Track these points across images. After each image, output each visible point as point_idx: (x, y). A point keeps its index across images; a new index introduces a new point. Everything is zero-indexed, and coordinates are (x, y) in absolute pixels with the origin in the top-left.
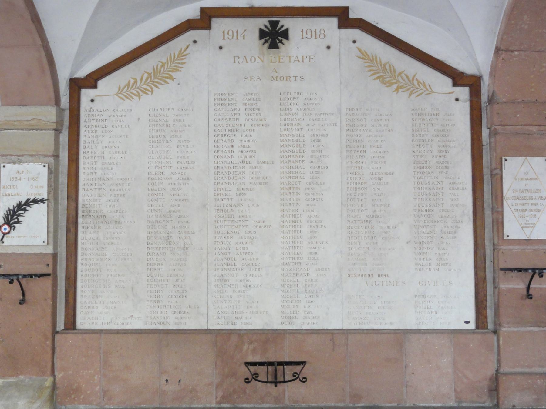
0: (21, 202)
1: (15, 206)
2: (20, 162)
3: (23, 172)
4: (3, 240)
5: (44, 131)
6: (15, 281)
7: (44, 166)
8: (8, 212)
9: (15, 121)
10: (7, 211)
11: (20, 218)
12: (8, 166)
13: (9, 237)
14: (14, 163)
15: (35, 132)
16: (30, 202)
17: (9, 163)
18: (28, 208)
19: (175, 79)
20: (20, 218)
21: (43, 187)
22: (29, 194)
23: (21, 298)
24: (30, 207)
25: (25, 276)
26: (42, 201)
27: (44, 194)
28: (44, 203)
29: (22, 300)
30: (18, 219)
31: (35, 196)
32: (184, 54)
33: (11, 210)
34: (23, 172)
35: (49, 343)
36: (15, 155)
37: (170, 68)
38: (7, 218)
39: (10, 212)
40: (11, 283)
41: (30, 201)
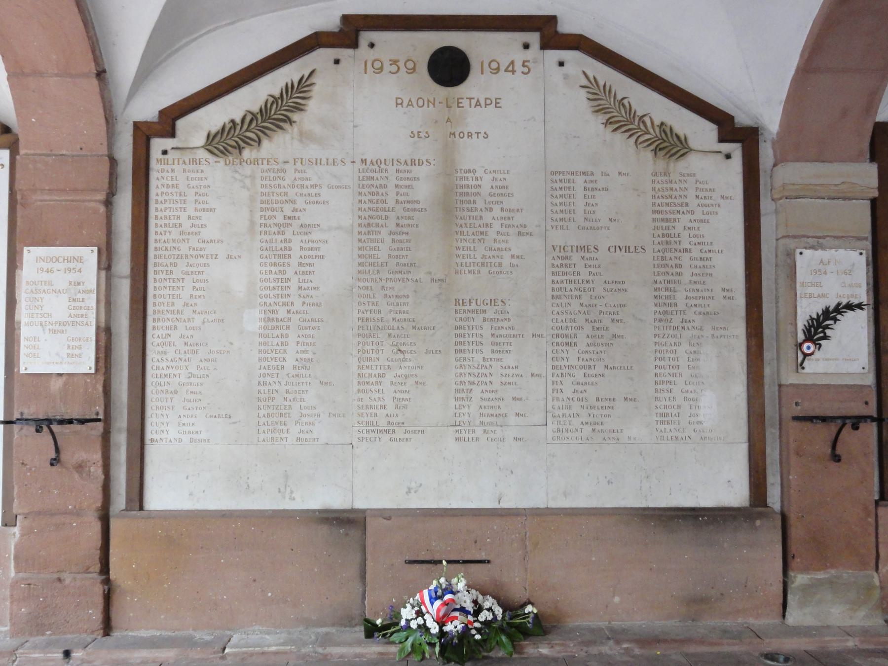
0: (829, 307)
1: (820, 314)
2: (822, 247)
3: (829, 262)
4: (804, 365)
5: (854, 201)
6: (45, 428)
7: (861, 254)
8: (810, 322)
9: (816, 185)
10: (808, 321)
11: (828, 332)
12: (807, 252)
13: (813, 360)
14: (812, 247)
15: (841, 202)
16: (843, 308)
17: (810, 248)
18: (839, 317)
19: (294, 122)
20: (828, 332)
21: (860, 286)
22: (840, 296)
23: (54, 455)
24: (842, 315)
25: (61, 422)
26: (860, 306)
27: (862, 294)
28: (862, 309)
29: (55, 459)
30: (825, 333)
31: (848, 298)
32: (308, 83)
33: (814, 319)
34: (829, 262)
35: (871, 520)
36: (813, 237)
37: (287, 106)
38: (809, 331)
39: (813, 322)
40: (37, 431)
41: (841, 306)
